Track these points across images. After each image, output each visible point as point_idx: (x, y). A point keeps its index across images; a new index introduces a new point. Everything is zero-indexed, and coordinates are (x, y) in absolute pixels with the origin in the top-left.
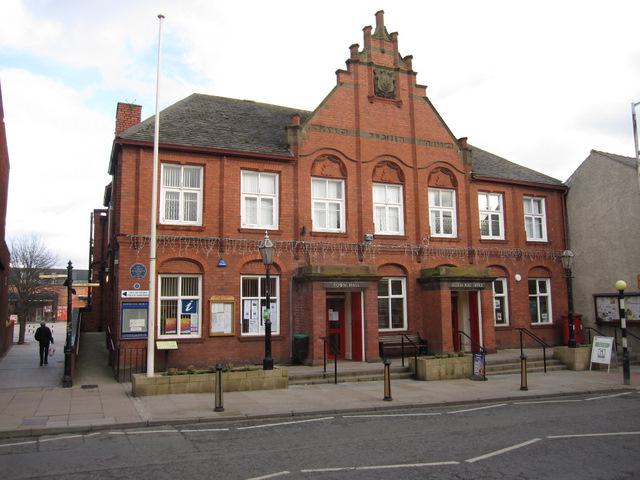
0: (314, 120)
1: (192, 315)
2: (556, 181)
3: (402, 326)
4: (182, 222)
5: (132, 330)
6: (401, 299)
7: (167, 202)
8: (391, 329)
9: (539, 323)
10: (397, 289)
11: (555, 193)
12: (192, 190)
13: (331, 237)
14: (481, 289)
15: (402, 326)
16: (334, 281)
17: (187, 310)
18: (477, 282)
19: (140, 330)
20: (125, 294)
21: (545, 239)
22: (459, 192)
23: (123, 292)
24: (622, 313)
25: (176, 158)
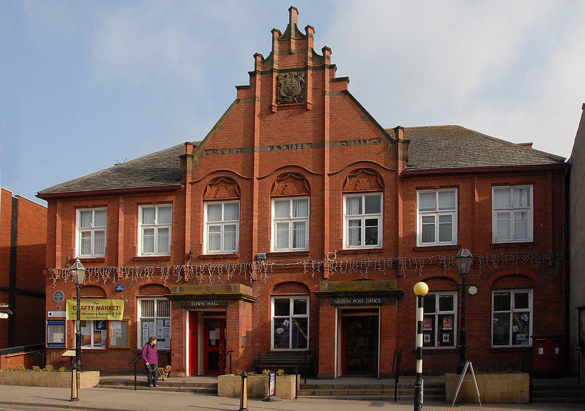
1: (102, 331)
2: (550, 157)
3: (306, 347)
4: (437, 243)
5: (54, 341)
6: (306, 319)
7: (210, 236)
8: (290, 349)
9: (511, 345)
10: (522, 301)
11: (549, 180)
12: (372, 217)
13: (219, 259)
14: (380, 304)
15: (306, 347)
16: (191, 300)
17: (99, 327)
18: (340, 297)
19: (60, 341)
20: (50, 314)
21: (78, 212)
22: (385, 194)
23: (49, 312)
24: (243, 347)
25: (431, 183)
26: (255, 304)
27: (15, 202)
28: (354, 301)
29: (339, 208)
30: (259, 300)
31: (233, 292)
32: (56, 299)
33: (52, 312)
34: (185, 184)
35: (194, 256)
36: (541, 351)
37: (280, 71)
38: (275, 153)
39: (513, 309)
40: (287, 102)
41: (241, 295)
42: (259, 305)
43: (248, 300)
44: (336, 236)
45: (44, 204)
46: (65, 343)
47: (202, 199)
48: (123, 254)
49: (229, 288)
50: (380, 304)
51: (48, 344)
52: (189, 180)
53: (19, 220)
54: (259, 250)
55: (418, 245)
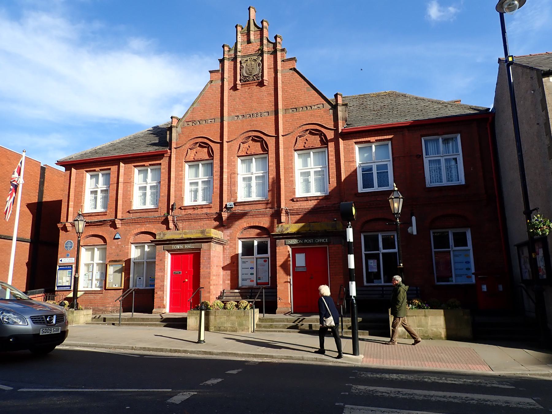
0: (187, 118)
10: (461, 241)
11: (474, 128)
20: (61, 261)
21: (462, 181)
23: (60, 259)
26: (225, 247)
27: (43, 169)
28: (306, 241)
29: (292, 163)
30: (229, 242)
31: (208, 235)
32: (66, 247)
33: (63, 259)
34: (170, 149)
35: (177, 206)
36: (484, 288)
37: (243, 57)
38: (240, 121)
39: (453, 248)
40: (248, 81)
41: (212, 238)
42: (228, 247)
43: (219, 242)
44: (290, 185)
45: (63, 169)
46: (70, 286)
47: (184, 160)
48: (121, 207)
49: (203, 232)
50: (328, 243)
51: (58, 287)
52: (174, 145)
53: (45, 184)
54: (229, 200)
55: (359, 191)
